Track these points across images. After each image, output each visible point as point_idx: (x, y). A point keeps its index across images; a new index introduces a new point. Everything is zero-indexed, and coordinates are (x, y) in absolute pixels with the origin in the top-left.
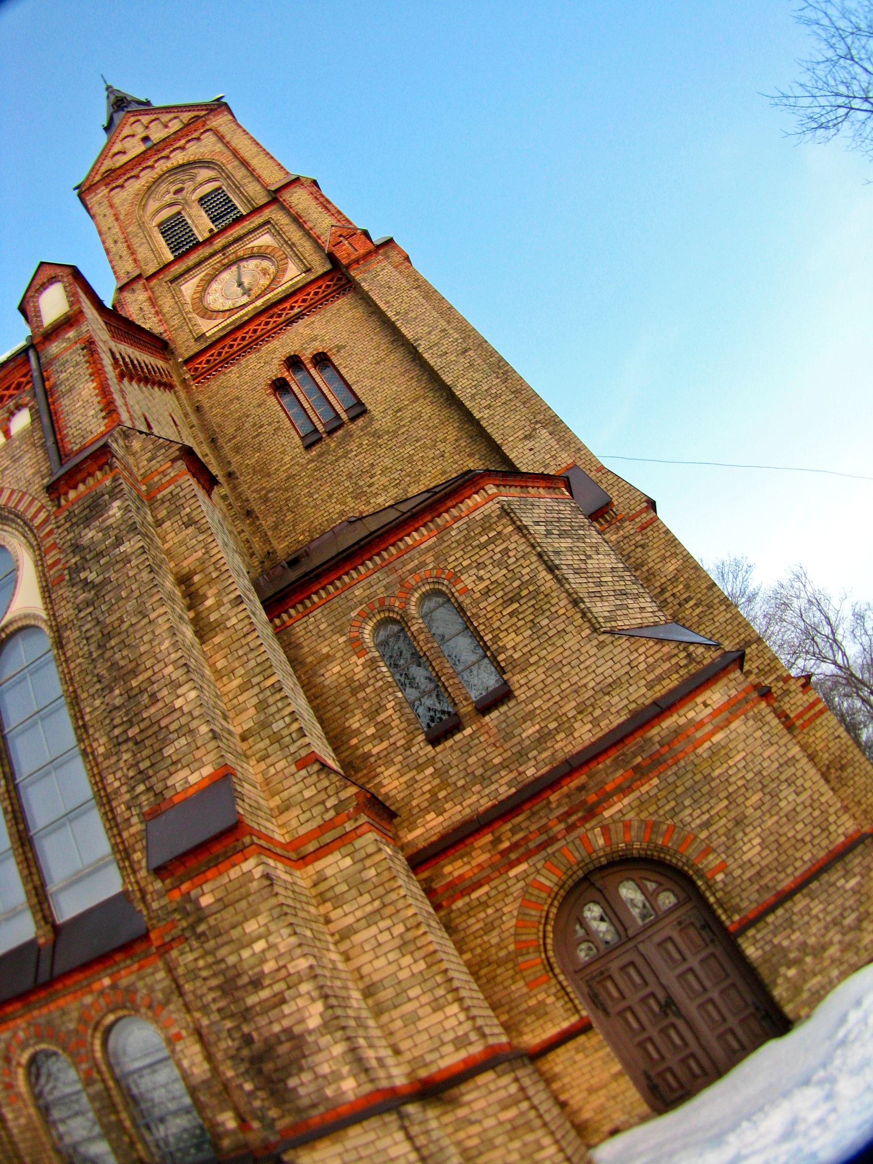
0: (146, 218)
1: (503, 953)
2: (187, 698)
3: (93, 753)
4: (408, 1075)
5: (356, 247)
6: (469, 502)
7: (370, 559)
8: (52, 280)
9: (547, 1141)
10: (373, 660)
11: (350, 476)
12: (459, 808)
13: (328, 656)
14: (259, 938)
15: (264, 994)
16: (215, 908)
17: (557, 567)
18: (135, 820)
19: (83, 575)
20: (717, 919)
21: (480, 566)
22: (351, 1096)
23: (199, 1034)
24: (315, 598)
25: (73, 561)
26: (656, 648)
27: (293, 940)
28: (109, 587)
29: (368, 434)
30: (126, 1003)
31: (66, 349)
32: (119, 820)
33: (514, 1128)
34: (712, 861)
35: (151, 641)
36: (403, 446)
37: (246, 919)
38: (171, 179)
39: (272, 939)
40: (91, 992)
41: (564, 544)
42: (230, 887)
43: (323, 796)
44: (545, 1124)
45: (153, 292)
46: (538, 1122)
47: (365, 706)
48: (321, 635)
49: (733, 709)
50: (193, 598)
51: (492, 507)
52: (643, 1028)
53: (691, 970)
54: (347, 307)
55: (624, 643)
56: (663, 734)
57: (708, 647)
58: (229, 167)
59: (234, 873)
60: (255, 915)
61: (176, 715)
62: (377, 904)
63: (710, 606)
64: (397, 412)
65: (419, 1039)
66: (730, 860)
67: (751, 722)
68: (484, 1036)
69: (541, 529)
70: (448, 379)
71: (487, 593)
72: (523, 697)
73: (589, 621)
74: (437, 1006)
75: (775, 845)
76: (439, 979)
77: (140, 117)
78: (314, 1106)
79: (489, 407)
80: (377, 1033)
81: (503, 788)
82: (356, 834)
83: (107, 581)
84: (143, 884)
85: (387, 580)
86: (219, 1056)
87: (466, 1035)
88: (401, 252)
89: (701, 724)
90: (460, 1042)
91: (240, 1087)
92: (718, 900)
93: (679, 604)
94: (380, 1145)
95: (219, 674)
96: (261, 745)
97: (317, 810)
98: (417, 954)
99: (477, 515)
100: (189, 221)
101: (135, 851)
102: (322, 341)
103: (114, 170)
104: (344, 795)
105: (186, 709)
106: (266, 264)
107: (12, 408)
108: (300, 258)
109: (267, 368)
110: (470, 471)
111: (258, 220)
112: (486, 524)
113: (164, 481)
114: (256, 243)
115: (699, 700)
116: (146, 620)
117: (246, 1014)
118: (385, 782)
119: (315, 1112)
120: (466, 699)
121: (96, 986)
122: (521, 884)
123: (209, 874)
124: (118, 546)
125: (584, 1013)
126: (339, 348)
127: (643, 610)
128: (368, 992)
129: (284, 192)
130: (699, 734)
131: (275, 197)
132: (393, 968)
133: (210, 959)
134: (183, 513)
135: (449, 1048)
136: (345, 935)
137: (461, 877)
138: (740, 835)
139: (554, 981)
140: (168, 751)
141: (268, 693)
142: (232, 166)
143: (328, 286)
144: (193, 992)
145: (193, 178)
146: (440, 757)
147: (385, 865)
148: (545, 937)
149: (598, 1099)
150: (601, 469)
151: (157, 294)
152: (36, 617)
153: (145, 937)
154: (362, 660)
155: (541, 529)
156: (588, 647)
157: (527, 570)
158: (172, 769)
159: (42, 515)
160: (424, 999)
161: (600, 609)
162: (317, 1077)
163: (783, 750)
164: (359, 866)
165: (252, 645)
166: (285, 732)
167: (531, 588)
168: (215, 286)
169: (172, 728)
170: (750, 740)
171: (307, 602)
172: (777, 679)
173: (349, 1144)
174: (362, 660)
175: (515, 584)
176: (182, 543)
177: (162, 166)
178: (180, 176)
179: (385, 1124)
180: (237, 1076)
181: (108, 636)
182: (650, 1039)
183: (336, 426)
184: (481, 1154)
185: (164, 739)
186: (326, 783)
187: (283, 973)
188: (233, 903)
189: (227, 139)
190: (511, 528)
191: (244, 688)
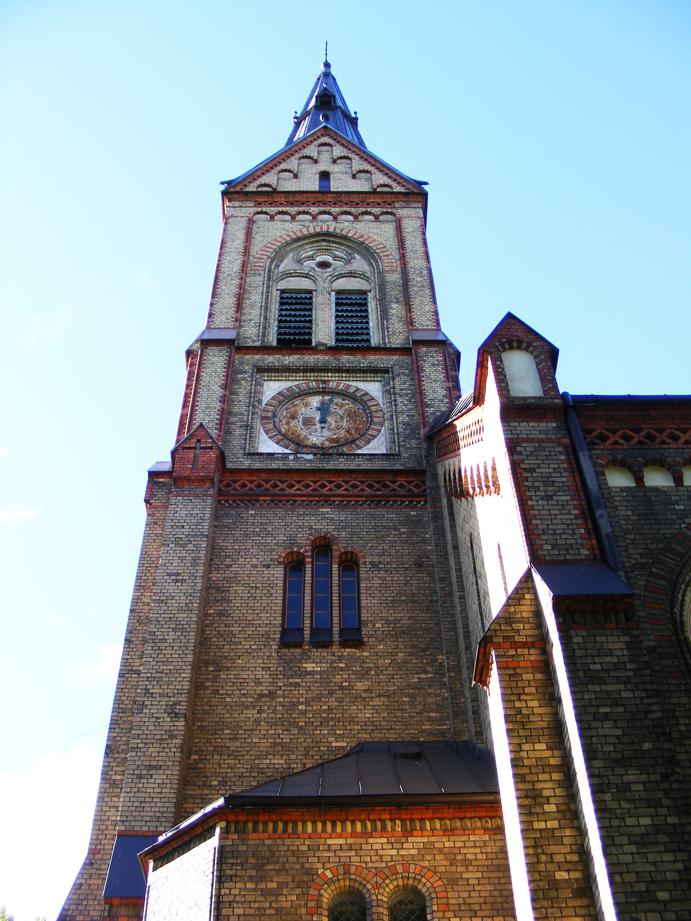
103: (275, 191)
114: (362, 385)
177: (326, 224)
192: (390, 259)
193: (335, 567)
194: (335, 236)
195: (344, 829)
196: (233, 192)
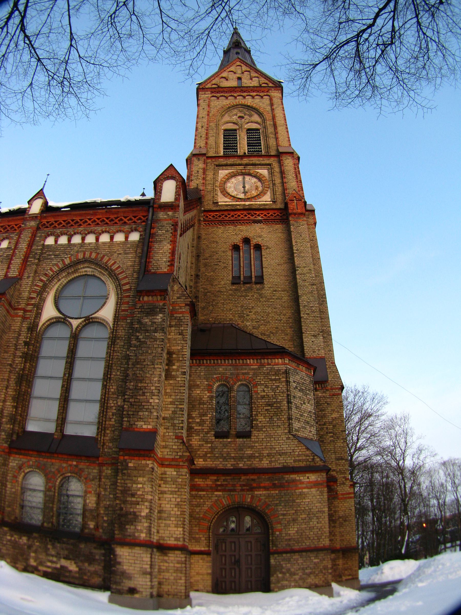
0: (221, 123)
1: (197, 516)
2: (155, 401)
3: (109, 389)
4: (157, 540)
5: (299, 207)
6: (276, 360)
7: (232, 360)
8: (172, 178)
9: (183, 578)
10: (212, 397)
11: (242, 306)
12: (212, 463)
13: (198, 385)
14: (141, 484)
15: (134, 499)
16: (132, 468)
17: (291, 403)
18: (113, 420)
19: (138, 334)
20: (269, 545)
21: (266, 386)
22: (142, 538)
23: (99, 495)
24: (205, 362)
25: (136, 326)
26: (305, 450)
27: (150, 489)
28: (145, 345)
29: (258, 293)
30: (78, 474)
31: (166, 220)
32: (108, 417)
33: (177, 570)
34: (279, 527)
35: (151, 374)
36: (269, 307)
37: (140, 477)
38: (241, 109)
39: (144, 486)
40: (67, 463)
41: (299, 394)
42: (140, 465)
43: (178, 450)
44: (186, 574)
45: (207, 166)
46: (184, 572)
47: (201, 411)
48: (199, 376)
49: (316, 484)
50: (170, 362)
51: (283, 368)
52: (225, 564)
53: (251, 555)
54: (280, 231)
55: (296, 442)
56: (289, 479)
57: (321, 460)
58: (268, 122)
59: (144, 462)
60: (144, 477)
61: (149, 404)
62: (177, 489)
63: (338, 438)
64: (274, 291)
65: (166, 532)
66: (284, 530)
67: (318, 492)
68: (184, 541)
69: (295, 385)
70: (300, 292)
71: (263, 397)
72: (253, 440)
73: (290, 428)
74: (177, 526)
75: (300, 534)
76: (182, 519)
77: (242, 65)
78: (130, 536)
79: (308, 314)
80: (156, 524)
81: (229, 465)
82: (182, 467)
83: (145, 343)
84: (105, 441)
85: (233, 371)
86: (102, 505)
87: (180, 538)
88: (315, 219)
89: (303, 483)
90: (177, 539)
91: (103, 517)
92: (272, 539)
93: (327, 433)
94: (142, 555)
95: (166, 394)
96: (168, 424)
97: (174, 454)
98: (180, 509)
99: (276, 367)
100: (238, 146)
101: (108, 430)
102: (263, 239)
104: (185, 454)
105: (152, 404)
106: (259, 184)
107: (133, 228)
108: (274, 193)
109: (235, 237)
110: (284, 348)
111: (266, 161)
112: (277, 373)
113: (180, 310)
115: (307, 475)
116: (153, 366)
117: (125, 502)
118: (193, 440)
119: (129, 538)
120: (235, 429)
121: (70, 463)
122: (217, 498)
123: (136, 458)
124: (155, 332)
125: (211, 549)
126: (268, 248)
127: (310, 432)
128: (160, 512)
129: (284, 155)
130: (300, 486)
131: (279, 155)
132: (171, 509)
133: (123, 481)
134: (181, 328)
135: (173, 539)
136: (163, 493)
137: (200, 484)
138: (292, 524)
139: (208, 534)
140: (141, 413)
141: (178, 409)
142: (269, 123)
143: (278, 215)
144: (104, 482)
145: (251, 116)
146: (215, 443)
147: (185, 480)
148: (213, 519)
149: (198, 578)
150: (333, 363)
151: (208, 168)
152: (108, 323)
153: (98, 458)
154: (208, 394)
155: (295, 385)
156: (284, 436)
157: (281, 398)
158: (139, 420)
159: (127, 287)
160: (174, 522)
161: (296, 425)
162: (136, 528)
163: (322, 507)
164: (177, 476)
165: (181, 391)
166: (177, 425)
167: (278, 405)
168: (233, 180)
169: (145, 407)
170: (314, 497)
171: (201, 361)
172: (344, 477)
173: (133, 551)
174: (208, 394)
175: (274, 400)
176: (175, 339)
177: (240, 100)
178: (245, 111)
179: (147, 551)
180: (104, 514)
181: (138, 363)
182: (225, 569)
183: (248, 280)
184: (164, 572)
185: (141, 409)
186: (181, 447)
187: (143, 496)
188: (138, 470)
189: (274, 107)
190: (284, 379)
191: (171, 403)
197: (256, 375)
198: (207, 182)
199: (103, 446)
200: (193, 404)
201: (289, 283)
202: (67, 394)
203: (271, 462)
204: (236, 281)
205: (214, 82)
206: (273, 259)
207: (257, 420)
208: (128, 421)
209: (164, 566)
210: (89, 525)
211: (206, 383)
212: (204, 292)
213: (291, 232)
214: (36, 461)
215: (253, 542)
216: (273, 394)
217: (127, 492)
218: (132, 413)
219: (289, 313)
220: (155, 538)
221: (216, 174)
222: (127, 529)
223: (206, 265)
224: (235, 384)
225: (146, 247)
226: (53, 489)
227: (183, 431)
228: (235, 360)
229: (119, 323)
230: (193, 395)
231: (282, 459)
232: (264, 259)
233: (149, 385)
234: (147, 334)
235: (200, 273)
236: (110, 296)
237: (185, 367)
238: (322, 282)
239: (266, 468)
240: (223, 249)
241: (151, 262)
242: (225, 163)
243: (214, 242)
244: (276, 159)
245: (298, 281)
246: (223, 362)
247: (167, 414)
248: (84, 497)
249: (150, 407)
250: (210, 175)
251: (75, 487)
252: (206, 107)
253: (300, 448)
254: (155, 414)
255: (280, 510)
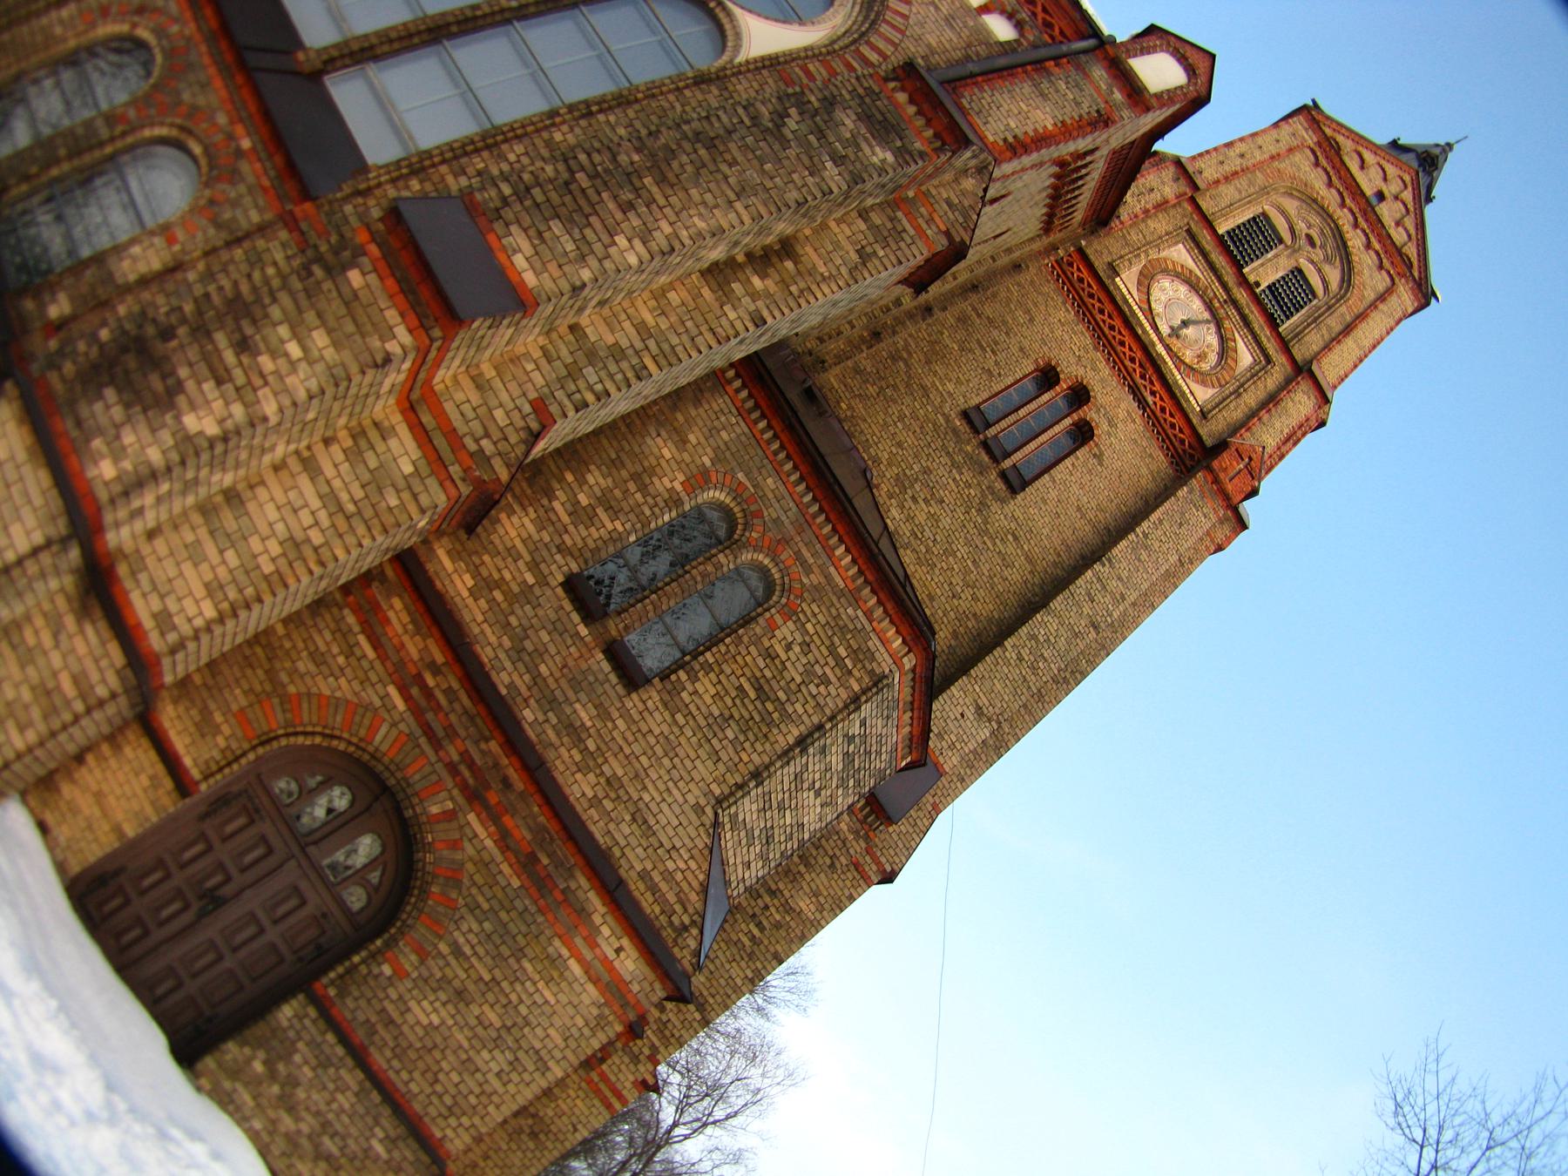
0: (1274, 197)
1: (284, 677)
2: (629, 252)
3: (554, 125)
4: (120, 550)
5: (1235, 481)
7: (815, 499)
8: (1190, 70)
10: (678, 502)
12: (480, 618)
13: (685, 441)
14: (304, 349)
15: (229, 356)
16: (346, 290)
17: (804, 751)
18: (464, 181)
19: (793, 111)
22: (91, 473)
23: (175, 268)
25: (813, 99)
26: (695, 884)
27: (302, 395)
28: (777, 147)
30: (216, 170)
31: (1098, 89)
32: (464, 160)
33: (48, 693)
34: (409, 960)
35: (704, 203)
36: (968, 543)
37: (329, 332)
38: (1327, 231)
39: (303, 365)
40: (232, 123)
41: (836, 760)
43: (496, 435)
44: (53, 734)
45: (1174, 206)
47: (617, 492)
48: (712, 432)
50: (762, 260)
51: (884, 663)
54: (1154, 467)
55: (703, 840)
56: (580, 893)
59: (392, 315)
60: (336, 344)
61: (605, 238)
62: (351, 508)
64: (1013, 535)
69: (856, 730)
70: (1057, 603)
71: (770, 655)
72: (629, 705)
73: (732, 794)
74: (213, 589)
76: (250, 591)
78: (79, 424)
79: (1020, 658)
80: (177, 507)
81: (506, 677)
82: (445, 480)
83: (785, 144)
84: (378, 192)
86: (146, 296)
87: (174, 628)
88: (1229, 540)
89: (593, 945)
90: (164, 620)
91: (104, 324)
92: (355, 967)
93: (754, 915)
94: (26, 512)
96: (564, 352)
97: (476, 426)
98: (282, 562)
100: (1256, 263)
101: (421, 182)
102: (1109, 434)
104: (497, 464)
105: (613, 250)
106: (1213, 358)
107: (1019, 16)
108: (1220, 403)
109: (1073, 360)
110: (934, 634)
111: (1272, 347)
112: (862, 655)
115: (625, 942)
116: (732, 196)
117: (201, 331)
118: (515, 519)
120: (626, 628)
121: (239, 130)
123: (390, 282)
126: (1099, 457)
127: (746, 864)
130: (579, 941)
131: (1303, 371)
132: (265, 530)
133: (276, 283)
135: (156, 605)
136: (309, 465)
137: (387, 621)
139: (246, 746)
140: (557, 227)
141: (635, 361)
143: (1182, 442)
144: (232, 261)
145: (1327, 260)
146: (549, 593)
147: (403, 518)
150: (937, 809)
151: (1172, 212)
152: (737, 48)
153: (306, 195)
154: (679, 488)
156: (697, 792)
157: (801, 711)
158: (532, 232)
159: (874, 57)
160: (222, 572)
161: (748, 808)
162: (118, 427)
164: (401, 484)
165: (699, 340)
166: (582, 384)
167: (776, 715)
168: (1183, 289)
169: (588, 232)
172: (653, 1047)
173: (27, 470)
174: (679, 488)
175: (781, 695)
176: (837, 245)
177: (1344, 219)
180: (119, 320)
181: (711, 145)
183: (994, 451)
184: (14, 647)
185: (572, 221)
186: (513, 439)
187: (258, 382)
191: (642, 328)
192: (1354, 304)
193: (1068, 421)
194: (1348, 255)
195: (797, 483)
196: (1310, 113)
197: (818, 593)
198: (1142, 226)
199: (359, 193)
200: (624, 457)
201: (1055, 564)
202: (454, 29)
203: (595, 802)
204: (974, 419)
205: (1340, 138)
206: (1082, 487)
207: (694, 678)
208: (505, 201)
209: (38, 634)
210: (54, 300)
211: (706, 460)
212: (897, 350)
213: (1173, 494)
214: (189, 39)
215: (308, 910)
216: (798, 680)
217: (242, 315)
218: (540, 198)
219: (987, 608)
220: (119, 536)
221: (1169, 238)
222: (101, 397)
223: (963, 319)
224: (757, 549)
225: (1001, 67)
226: (119, 129)
227: (571, 413)
228: (821, 510)
229: (765, 72)
230: (649, 440)
231: (627, 831)
232: (1068, 462)
233: (667, 210)
234: (811, 137)
235: (938, 314)
236: (810, 28)
237: (777, 313)
238: (1104, 649)
239: (565, 798)
240: (1026, 343)
241: (982, 90)
242: (1208, 248)
243: (1028, 312)
244: (1289, 368)
245: (1080, 582)
246: (793, 478)
247: (597, 331)
248: (145, 233)
249: (598, 247)
250: (1160, 225)
251: (167, 188)
252: (1283, 147)
253: (693, 864)
254: (586, 275)
255: (465, 927)
